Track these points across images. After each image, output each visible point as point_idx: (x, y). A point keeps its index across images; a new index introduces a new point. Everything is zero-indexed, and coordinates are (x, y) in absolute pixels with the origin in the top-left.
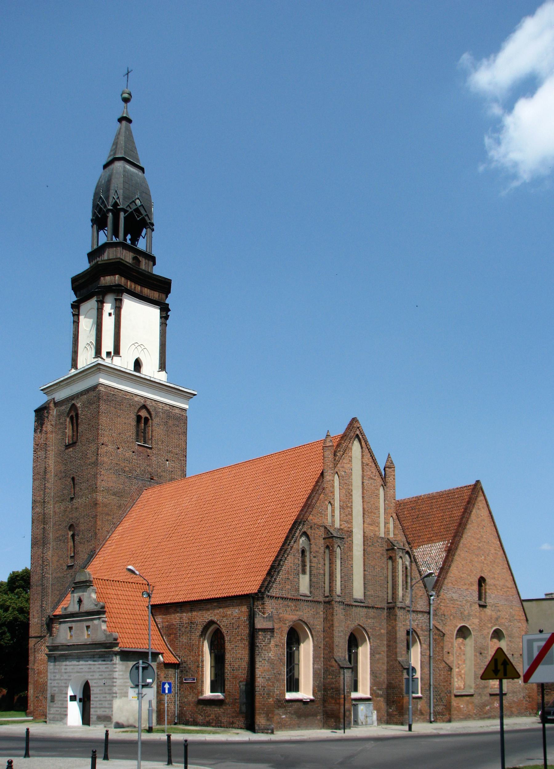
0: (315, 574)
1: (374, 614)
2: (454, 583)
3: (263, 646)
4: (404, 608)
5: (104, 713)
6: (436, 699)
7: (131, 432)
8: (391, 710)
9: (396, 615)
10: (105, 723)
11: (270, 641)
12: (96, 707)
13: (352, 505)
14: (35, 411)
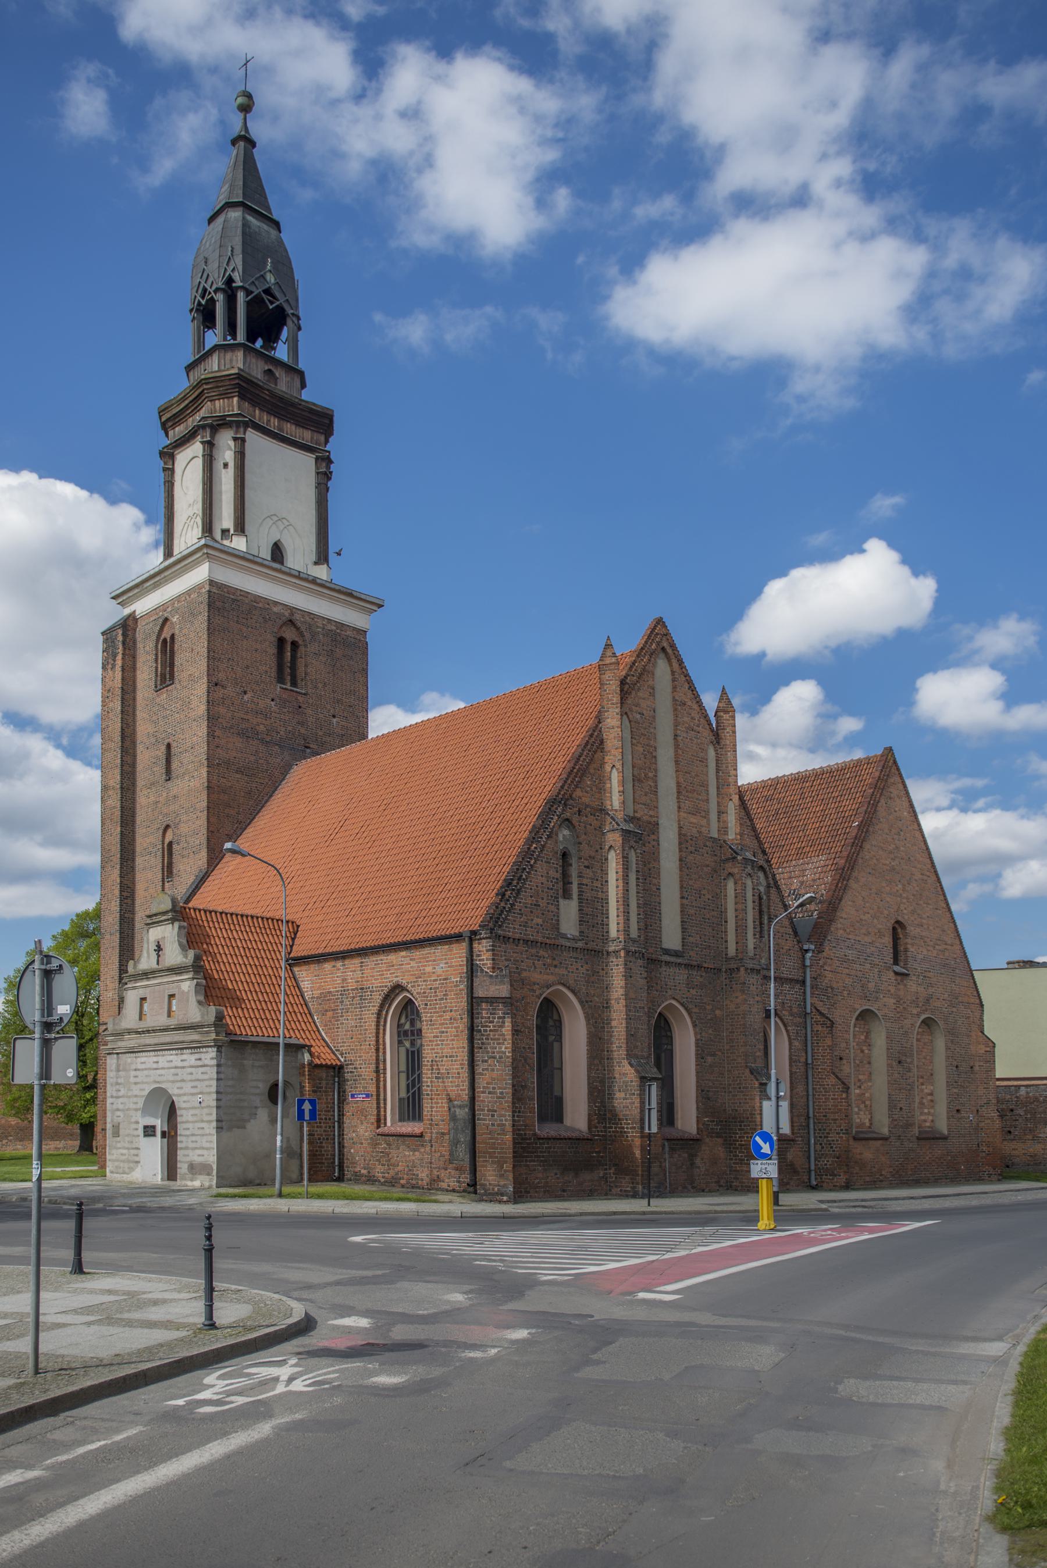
1: (701, 980)
2: (848, 930)
3: (490, 1031)
4: (758, 971)
7: (268, 663)
11: (503, 1022)
12: (187, 1148)
13: (656, 776)
14: (103, 633)
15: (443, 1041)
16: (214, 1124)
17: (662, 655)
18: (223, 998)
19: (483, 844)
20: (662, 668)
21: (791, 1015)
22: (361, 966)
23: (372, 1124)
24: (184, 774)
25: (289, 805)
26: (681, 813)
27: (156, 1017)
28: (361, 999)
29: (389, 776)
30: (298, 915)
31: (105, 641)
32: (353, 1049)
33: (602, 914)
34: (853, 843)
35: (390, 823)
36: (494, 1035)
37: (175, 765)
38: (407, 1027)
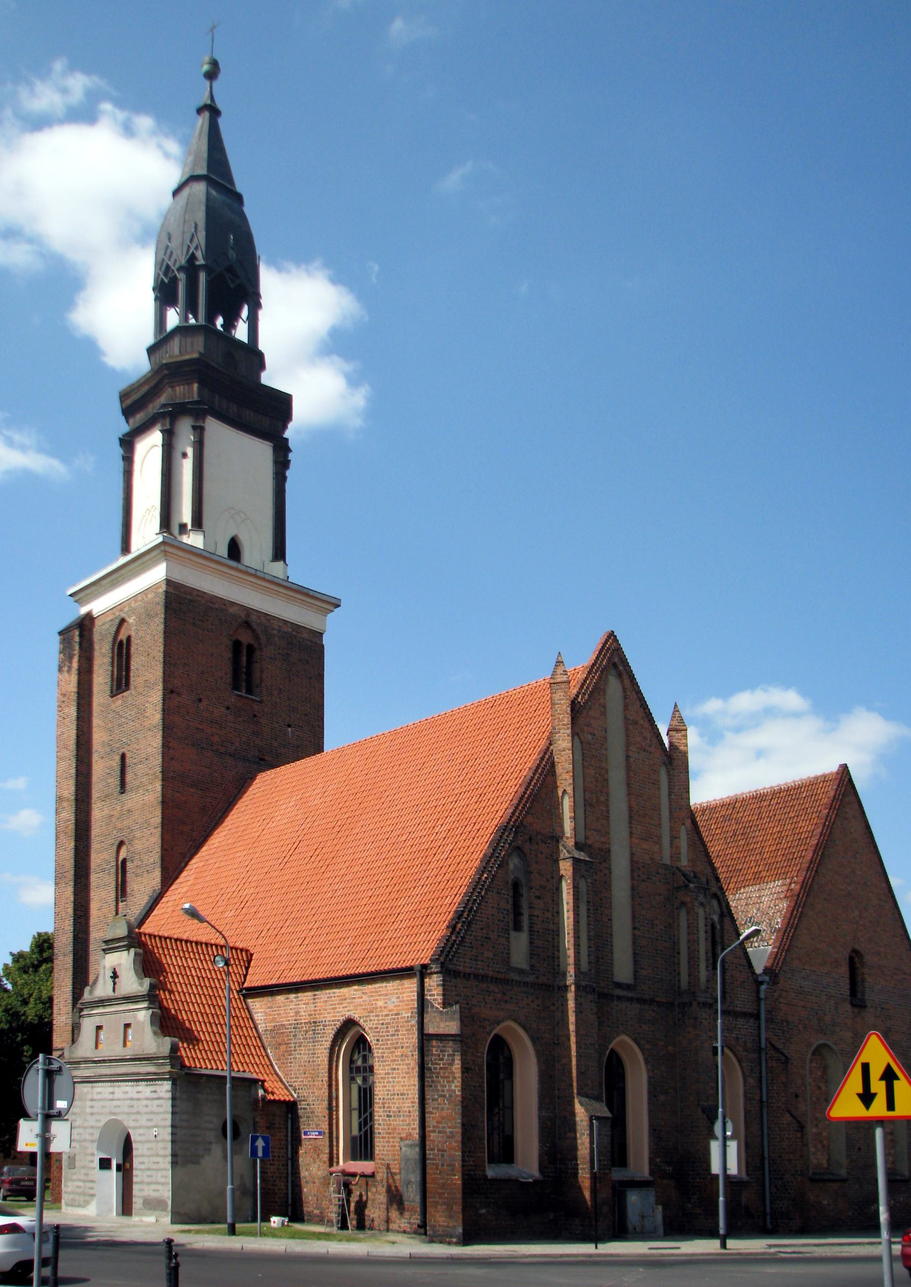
0: (540, 930)
3: (441, 1068)
5: (155, 1195)
6: (776, 1186)
8: (690, 1206)
9: (696, 1018)
10: (157, 1213)
11: (453, 1060)
13: (607, 800)
14: (60, 633)
15: (395, 1078)
16: (169, 1159)
17: (613, 671)
18: (177, 1029)
19: (435, 872)
20: (614, 686)
21: (746, 1050)
22: (314, 999)
23: (325, 1162)
24: (138, 787)
25: (244, 823)
26: (633, 839)
27: (111, 1047)
28: (314, 1034)
29: (344, 794)
30: (252, 943)
31: (63, 642)
32: (306, 1085)
33: (553, 946)
34: (809, 867)
35: (344, 846)
36: (444, 1073)
37: (129, 777)
38: (359, 1063)
